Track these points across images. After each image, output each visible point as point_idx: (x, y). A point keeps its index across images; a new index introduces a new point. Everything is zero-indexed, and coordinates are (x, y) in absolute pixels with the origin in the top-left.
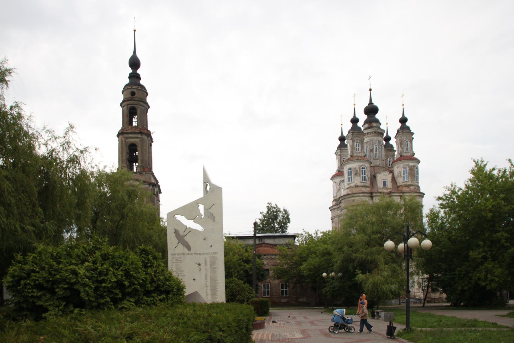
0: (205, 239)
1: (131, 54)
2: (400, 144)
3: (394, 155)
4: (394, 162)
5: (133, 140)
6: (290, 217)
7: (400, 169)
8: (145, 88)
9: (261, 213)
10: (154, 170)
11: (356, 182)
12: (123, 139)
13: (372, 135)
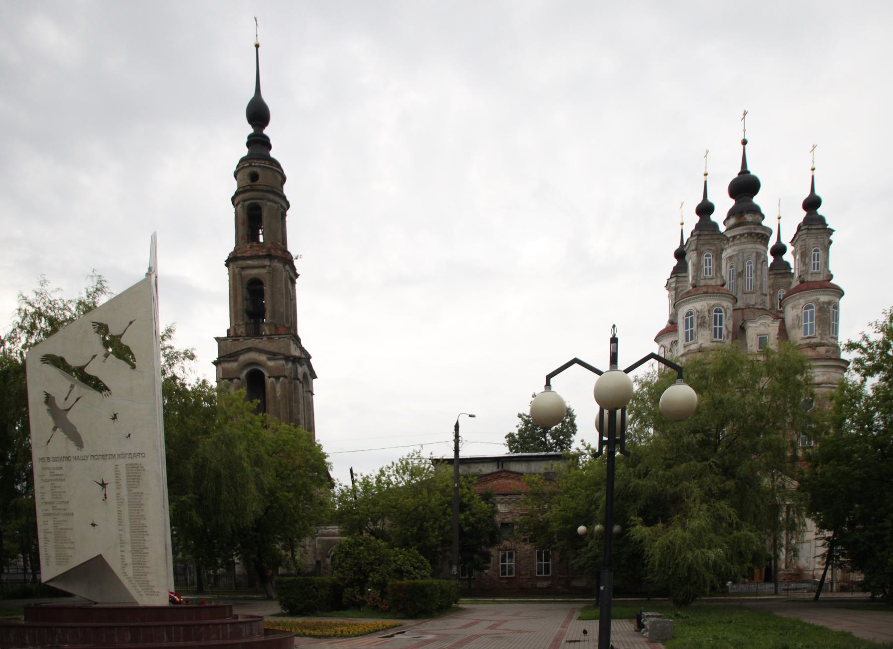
0: (115, 417)
1: (251, 94)
2: (803, 255)
3: (790, 283)
4: (790, 293)
5: (254, 272)
6: (576, 422)
7: (799, 311)
8: (278, 165)
9: (520, 416)
10: (301, 332)
11: (700, 341)
12: (237, 270)
13: (743, 240)
